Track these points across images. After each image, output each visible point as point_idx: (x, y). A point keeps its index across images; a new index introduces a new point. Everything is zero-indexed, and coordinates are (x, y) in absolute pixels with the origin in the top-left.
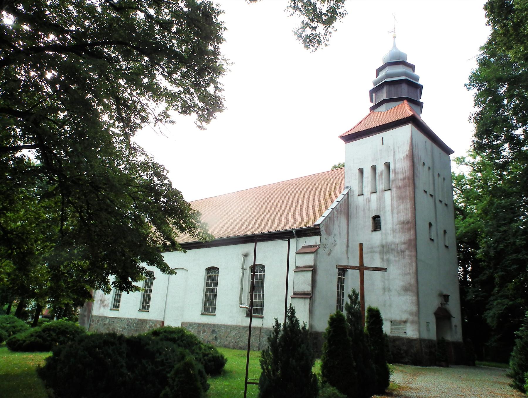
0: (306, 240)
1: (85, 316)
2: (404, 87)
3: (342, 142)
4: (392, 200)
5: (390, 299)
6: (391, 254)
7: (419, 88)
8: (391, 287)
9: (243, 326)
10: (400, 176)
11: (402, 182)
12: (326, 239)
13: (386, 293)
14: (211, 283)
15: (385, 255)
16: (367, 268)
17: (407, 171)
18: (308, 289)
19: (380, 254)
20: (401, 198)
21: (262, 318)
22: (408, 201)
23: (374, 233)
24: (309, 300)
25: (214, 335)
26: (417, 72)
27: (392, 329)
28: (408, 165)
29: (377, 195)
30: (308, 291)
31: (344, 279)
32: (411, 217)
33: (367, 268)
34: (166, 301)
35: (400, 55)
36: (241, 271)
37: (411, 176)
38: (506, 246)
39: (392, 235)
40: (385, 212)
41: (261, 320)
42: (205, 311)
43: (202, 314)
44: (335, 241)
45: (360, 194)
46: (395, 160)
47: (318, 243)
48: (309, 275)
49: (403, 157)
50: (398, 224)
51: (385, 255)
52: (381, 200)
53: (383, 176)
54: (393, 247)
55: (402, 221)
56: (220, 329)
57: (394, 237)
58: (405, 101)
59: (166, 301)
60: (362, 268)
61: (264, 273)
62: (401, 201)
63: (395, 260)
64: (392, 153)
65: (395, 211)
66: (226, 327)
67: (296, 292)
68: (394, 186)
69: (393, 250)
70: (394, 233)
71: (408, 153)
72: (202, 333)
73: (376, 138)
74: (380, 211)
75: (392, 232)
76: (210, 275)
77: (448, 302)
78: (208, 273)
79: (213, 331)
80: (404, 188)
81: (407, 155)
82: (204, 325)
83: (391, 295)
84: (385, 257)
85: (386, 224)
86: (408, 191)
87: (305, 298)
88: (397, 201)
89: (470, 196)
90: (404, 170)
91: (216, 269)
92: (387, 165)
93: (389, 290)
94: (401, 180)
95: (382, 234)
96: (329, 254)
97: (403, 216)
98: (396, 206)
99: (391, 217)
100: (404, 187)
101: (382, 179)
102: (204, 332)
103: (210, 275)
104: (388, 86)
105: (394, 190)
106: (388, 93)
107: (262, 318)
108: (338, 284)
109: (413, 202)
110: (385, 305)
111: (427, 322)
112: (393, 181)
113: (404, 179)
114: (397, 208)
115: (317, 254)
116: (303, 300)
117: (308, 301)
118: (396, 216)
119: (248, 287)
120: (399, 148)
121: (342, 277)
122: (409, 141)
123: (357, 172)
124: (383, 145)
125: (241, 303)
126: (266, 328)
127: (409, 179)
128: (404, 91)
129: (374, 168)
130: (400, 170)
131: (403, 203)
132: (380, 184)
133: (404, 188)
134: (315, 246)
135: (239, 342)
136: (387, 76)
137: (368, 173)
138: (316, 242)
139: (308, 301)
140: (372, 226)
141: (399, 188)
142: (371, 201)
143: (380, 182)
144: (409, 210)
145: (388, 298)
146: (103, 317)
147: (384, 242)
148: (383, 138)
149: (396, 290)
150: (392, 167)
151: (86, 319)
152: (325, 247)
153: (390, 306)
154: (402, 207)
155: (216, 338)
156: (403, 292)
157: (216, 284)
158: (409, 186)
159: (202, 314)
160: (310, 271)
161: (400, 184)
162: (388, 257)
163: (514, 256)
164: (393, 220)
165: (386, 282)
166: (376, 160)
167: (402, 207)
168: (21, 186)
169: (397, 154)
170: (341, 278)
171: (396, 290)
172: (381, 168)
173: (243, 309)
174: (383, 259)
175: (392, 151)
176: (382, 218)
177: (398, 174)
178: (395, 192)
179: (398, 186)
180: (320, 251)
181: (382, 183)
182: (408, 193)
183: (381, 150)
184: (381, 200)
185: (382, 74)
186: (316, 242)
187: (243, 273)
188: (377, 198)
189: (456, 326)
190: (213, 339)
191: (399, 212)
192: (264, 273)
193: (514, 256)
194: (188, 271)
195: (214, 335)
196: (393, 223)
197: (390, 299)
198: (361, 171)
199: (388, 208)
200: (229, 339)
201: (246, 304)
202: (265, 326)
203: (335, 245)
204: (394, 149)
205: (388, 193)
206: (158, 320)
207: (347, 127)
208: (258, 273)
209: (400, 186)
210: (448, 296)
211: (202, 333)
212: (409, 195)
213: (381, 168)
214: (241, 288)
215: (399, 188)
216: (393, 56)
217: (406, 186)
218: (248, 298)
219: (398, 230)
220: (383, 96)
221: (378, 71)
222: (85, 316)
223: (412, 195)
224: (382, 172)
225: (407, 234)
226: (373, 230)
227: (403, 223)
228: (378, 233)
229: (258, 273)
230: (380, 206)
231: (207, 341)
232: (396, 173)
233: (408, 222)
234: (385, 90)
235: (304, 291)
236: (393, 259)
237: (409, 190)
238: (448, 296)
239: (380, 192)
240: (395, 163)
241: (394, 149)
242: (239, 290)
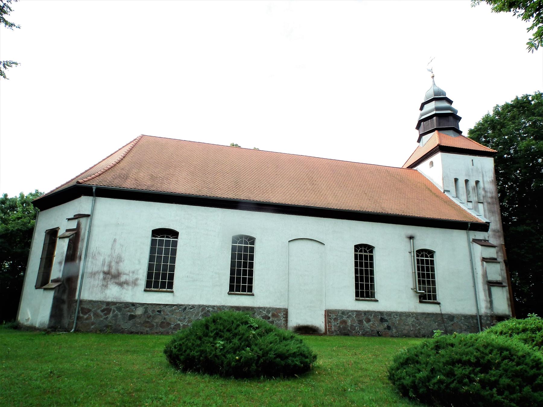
0: (476, 234)
1: (63, 302)
4: (484, 211)
10: (489, 195)
17: (493, 193)
21: (172, 292)
22: (497, 215)
25: (385, 325)
28: (494, 188)
29: (472, 204)
30: (500, 281)
32: (500, 228)
41: (438, 306)
49: (490, 181)
56: (391, 316)
67: (490, 280)
71: (493, 179)
72: (365, 322)
73: (468, 158)
81: (492, 181)
82: (366, 313)
88: (488, 214)
90: (491, 191)
92: (477, 182)
94: (490, 198)
97: (494, 225)
106: (439, 123)
107: (172, 292)
108: (356, 276)
120: (486, 173)
129: (467, 181)
131: (493, 216)
132: (474, 196)
135: (419, 329)
136: (437, 109)
137: (461, 183)
146: (121, 303)
150: (481, 184)
151: (65, 307)
156: (123, 287)
169: (485, 177)
172: (472, 183)
181: (475, 196)
182: (496, 209)
183: (472, 170)
186: (485, 237)
188: (473, 206)
190: (385, 329)
194: (324, 244)
195: (385, 325)
198: (456, 180)
200: (407, 327)
204: (482, 172)
206: (281, 307)
211: (365, 322)
212: (497, 211)
213: (472, 183)
215: (489, 203)
222: (63, 302)
225: (498, 239)
231: (376, 332)
233: (498, 232)
235: (497, 281)
239: (474, 203)
241: (482, 172)
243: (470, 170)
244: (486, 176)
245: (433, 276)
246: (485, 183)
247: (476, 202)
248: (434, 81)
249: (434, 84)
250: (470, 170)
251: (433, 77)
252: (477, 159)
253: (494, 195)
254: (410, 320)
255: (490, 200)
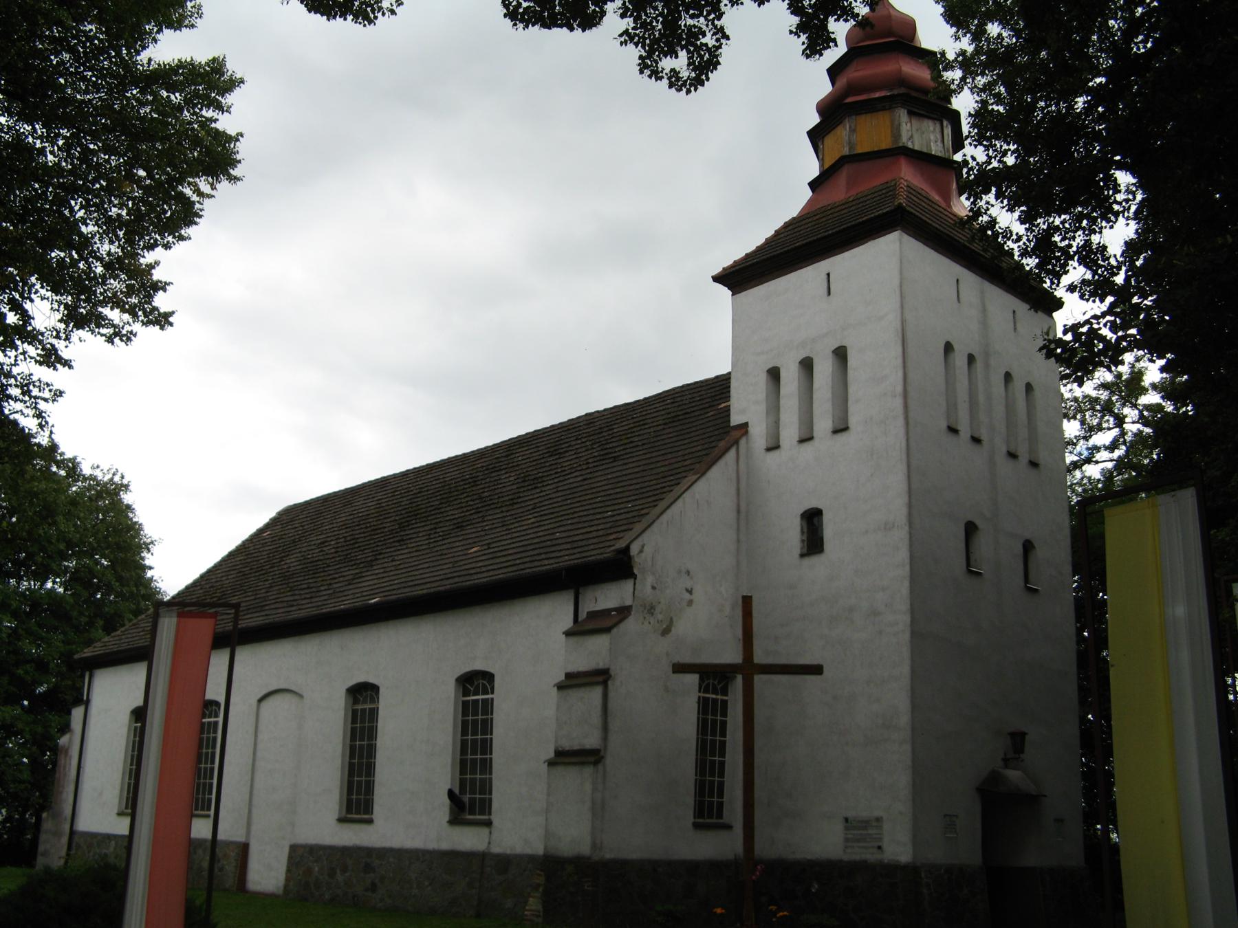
12: (654, 588)
14: (475, 722)
21: (488, 824)
27: (847, 840)
31: (725, 703)
34: (252, 786)
41: (485, 831)
42: (349, 810)
43: (341, 820)
44: (690, 591)
45: (769, 446)
47: (628, 602)
59: (252, 786)
61: (216, 719)
66: (399, 853)
76: (359, 707)
77: (1022, 752)
78: (356, 701)
79: (368, 868)
82: (345, 851)
87: (582, 763)
89: (78, 555)
91: (488, 677)
96: (666, 631)
102: (344, 870)
103: (359, 707)
111: (945, 816)
117: (588, 771)
121: (719, 697)
123: (763, 378)
124: (829, 293)
126: (498, 855)
129: (807, 365)
140: (803, 541)
148: (828, 275)
152: (651, 610)
155: (373, 888)
157: (487, 727)
159: (341, 820)
160: (597, 683)
170: (715, 701)
189: (1059, 821)
190: (367, 890)
192: (216, 719)
194: (301, 696)
198: (774, 374)
203: (690, 603)
210: (1023, 735)
226: (805, 551)
228: (814, 560)
238: (1023, 735)
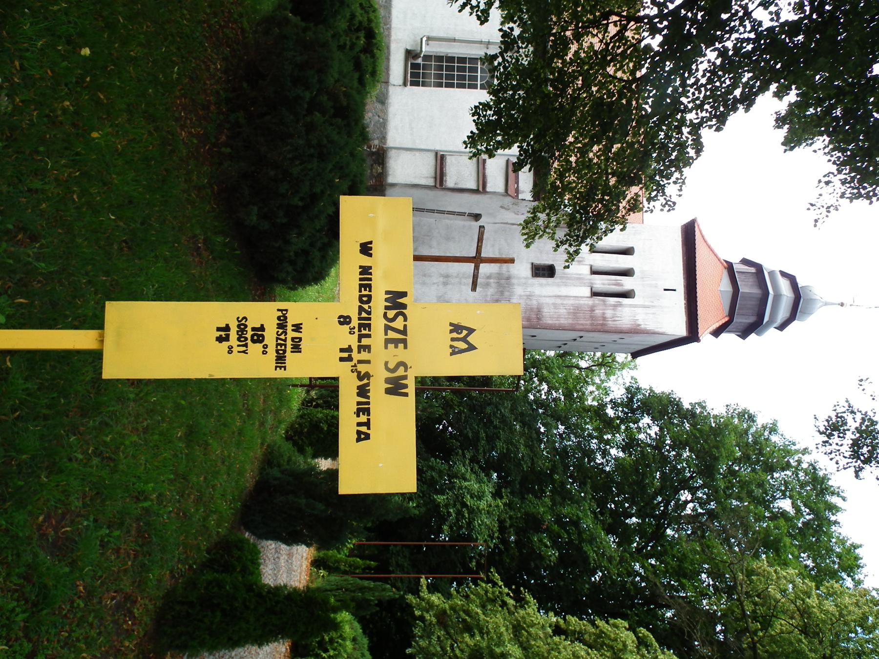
2: (751, 319)
3: (686, 220)
5: (434, 284)
6: (496, 290)
7: (744, 334)
8: (449, 287)
9: (389, 43)
10: (609, 313)
11: (599, 315)
13: (441, 279)
15: (496, 281)
16: (477, 268)
17: (615, 323)
18: (450, 182)
19: (497, 273)
20: (576, 311)
21: (405, 84)
22: (570, 321)
23: (530, 266)
24: (433, 184)
26: (772, 333)
28: (624, 326)
30: (446, 181)
32: (545, 324)
33: (477, 268)
35: (807, 312)
36: (485, 39)
37: (606, 328)
38: (495, 427)
39: (523, 294)
40: (558, 285)
41: (401, 82)
46: (635, 306)
47: (521, 196)
48: (472, 185)
50: (539, 304)
51: (496, 281)
52: (579, 279)
53: (614, 287)
54: (506, 294)
55: (542, 310)
57: (520, 296)
58: (727, 319)
60: (477, 260)
62: (572, 311)
63: (487, 295)
64: (647, 303)
65: (559, 301)
68: (597, 302)
69: (502, 293)
70: (525, 297)
71: (642, 327)
73: (678, 281)
74: (561, 278)
75: (528, 293)
80: (591, 317)
81: (639, 325)
83: (438, 285)
84: (492, 281)
85: (541, 285)
86: (585, 322)
87: (436, 178)
90: (617, 319)
93: (445, 284)
94: (604, 314)
95: (526, 278)
96: (502, 207)
98: (565, 302)
99: (551, 294)
100: (592, 318)
101: (609, 285)
104: (760, 296)
105: (591, 302)
106: (747, 296)
107: (405, 84)
109: (568, 328)
110: (425, 275)
112: (604, 301)
113: (604, 319)
114: (562, 304)
115: (503, 195)
116: (433, 174)
117: (431, 182)
118: (551, 302)
119: (456, 53)
120: (653, 314)
122: (661, 331)
125: (429, 39)
127: (602, 325)
128: (741, 320)
129: (627, 273)
130: (618, 313)
131: (569, 313)
133: (591, 317)
134: (517, 191)
136: (778, 297)
137: (622, 262)
138: (523, 192)
139: (431, 182)
141: (592, 310)
142: (579, 264)
143: (606, 282)
144: (557, 322)
145: (435, 281)
147: (514, 281)
149: (445, 293)
153: (424, 283)
154: (563, 311)
158: (592, 324)
160: (478, 186)
161: (597, 311)
162: (493, 285)
163: (483, 435)
164: (544, 297)
165: (457, 280)
166: (642, 278)
167: (563, 311)
168: (649, 445)
171: (445, 293)
172: (627, 283)
173: (419, 41)
174: (489, 277)
175: (650, 304)
176: (550, 280)
177: (613, 309)
178: (586, 302)
179: (595, 308)
180: (509, 199)
181: (604, 284)
184: (579, 279)
185: (784, 286)
186: (523, 192)
187: (481, 42)
191: (555, 306)
193: (483, 435)
196: (540, 296)
197: (434, 284)
199: (564, 291)
201: (428, 49)
202: (391, 89)
204: (653, 306)
205: (587, 292)
207: (706, 231)
208: (479, 74)
209: (594, 311)
213: (627, 283)
214: (454, 40)
215: (592, 310)
216: (811, 301)
217: (592, 320)
218: (436, 52)
219: (529, 303)
220: (747, 288)
221: (792, 280)
223: (578, 327)
224: (622, 285)
227: (539, 311)
228: (528, 273)
229: (479, 74)
230: (568, 278)
232: (615, 306)
233: (539, 319)
234: (756, 291)
236: (489, 293)
237: (586, 324)
239: (590, 280)
240: (631, 306)
241: (653, 306)
242: (450, 35)
243: (654, 282)
244: (647, 314)
245: (450, 85)
246: (633, 309)
247: (592, 284)
248: (835, 304)
249: (826, 304)
250: (654, 282)
251: (842, 305)
252: (679, 299)
253: (610, 322)
254: (371, 498)
255: (598, 312)
